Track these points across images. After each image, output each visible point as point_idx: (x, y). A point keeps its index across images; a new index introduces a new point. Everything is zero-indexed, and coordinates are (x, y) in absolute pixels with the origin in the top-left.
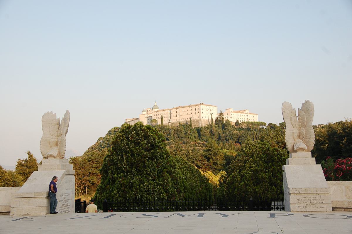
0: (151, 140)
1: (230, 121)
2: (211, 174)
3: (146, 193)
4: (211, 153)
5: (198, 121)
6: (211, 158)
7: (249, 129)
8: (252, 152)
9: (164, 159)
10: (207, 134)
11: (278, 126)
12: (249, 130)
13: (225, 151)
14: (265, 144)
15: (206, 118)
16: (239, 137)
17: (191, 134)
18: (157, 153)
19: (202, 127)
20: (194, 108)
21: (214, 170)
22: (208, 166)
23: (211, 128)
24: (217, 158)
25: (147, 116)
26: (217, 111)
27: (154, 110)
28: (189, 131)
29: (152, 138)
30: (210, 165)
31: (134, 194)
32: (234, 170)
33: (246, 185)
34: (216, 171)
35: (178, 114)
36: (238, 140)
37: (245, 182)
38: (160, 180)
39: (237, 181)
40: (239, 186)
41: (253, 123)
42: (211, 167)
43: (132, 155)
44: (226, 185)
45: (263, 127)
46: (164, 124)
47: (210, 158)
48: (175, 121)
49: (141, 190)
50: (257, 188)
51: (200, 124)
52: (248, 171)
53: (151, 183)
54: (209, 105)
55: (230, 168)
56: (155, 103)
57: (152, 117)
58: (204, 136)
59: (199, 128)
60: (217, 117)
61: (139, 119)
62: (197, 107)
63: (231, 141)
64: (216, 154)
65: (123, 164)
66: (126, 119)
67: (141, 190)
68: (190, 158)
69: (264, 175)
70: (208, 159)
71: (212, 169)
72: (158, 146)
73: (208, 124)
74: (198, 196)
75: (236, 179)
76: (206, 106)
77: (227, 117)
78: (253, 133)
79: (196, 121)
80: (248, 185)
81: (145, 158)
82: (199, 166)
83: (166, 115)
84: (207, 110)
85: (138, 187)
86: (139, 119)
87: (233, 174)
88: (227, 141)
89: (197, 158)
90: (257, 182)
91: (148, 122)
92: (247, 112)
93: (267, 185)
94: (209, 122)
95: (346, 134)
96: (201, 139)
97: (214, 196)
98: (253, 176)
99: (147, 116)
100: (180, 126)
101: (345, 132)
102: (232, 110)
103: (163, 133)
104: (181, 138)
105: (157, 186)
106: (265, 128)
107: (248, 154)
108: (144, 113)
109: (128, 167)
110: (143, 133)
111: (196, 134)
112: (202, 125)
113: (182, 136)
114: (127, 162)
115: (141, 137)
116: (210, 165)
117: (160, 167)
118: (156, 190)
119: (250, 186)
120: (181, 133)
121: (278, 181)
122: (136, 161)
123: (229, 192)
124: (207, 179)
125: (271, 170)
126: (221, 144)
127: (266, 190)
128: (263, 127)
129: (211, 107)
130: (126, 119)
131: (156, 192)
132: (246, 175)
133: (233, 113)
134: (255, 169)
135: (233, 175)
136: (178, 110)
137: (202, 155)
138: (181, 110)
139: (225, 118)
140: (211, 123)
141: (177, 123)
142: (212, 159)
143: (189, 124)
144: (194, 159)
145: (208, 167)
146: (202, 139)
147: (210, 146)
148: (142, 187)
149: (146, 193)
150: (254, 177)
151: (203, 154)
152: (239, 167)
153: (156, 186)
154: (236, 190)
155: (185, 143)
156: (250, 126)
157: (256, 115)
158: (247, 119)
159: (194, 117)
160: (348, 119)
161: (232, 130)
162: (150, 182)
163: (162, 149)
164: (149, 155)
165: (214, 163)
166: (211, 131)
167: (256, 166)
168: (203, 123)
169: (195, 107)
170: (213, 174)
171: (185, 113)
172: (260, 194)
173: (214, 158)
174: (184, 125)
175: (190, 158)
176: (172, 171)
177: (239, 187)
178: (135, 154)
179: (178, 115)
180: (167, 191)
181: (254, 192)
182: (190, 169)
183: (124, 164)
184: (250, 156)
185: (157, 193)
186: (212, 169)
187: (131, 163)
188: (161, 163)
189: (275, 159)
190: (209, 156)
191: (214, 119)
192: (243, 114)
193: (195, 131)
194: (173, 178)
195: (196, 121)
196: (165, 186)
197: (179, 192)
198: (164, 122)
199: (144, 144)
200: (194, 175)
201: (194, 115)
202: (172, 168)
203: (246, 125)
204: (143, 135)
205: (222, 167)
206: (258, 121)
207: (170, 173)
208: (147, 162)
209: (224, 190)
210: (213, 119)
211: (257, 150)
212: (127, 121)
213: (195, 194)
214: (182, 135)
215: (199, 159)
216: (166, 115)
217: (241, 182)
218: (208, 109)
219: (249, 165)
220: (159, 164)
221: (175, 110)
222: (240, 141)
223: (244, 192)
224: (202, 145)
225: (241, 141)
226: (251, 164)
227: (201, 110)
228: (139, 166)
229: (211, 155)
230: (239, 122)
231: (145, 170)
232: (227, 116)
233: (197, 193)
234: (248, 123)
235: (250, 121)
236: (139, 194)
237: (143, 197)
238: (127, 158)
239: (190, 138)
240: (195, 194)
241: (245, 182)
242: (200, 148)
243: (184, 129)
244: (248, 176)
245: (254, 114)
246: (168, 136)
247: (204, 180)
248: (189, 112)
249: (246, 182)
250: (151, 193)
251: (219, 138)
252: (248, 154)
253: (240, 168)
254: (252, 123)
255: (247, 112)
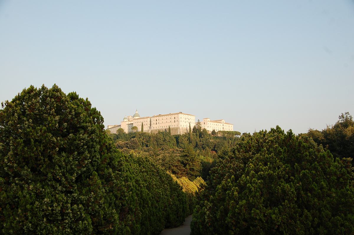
0: (70, 116)
1: (207, 130)
2: (186, 180)
3: (45, 220)
4: (188, 158)
5: (176, 129)
6: (188, 163)
7: (224, 138)
8: (256, 143)
9: (95, 151)
10: (186, 142)
11: (252, 135)
12: (224, 139)
13: (202, 157)
14: (278, 131)
15: (185, 127)
16: (215, 145)
17: (169, 141)
18: (80, 140)
19: (180, 135)
20: (173, 117)
21: (190, 176)
22: (185, 172)
23: (189, 136)
24: (194, 164)
25: (128, 123)
26: (195, 120)
27: (135, 118)
28: (167, 138)
29: (73, 113)
30: (187, 171)
31: (19, 222)
32: (225, 175)
33: (250, 206)
34: (192, 178)
35: (157, 122)
36: (214, 148)
37: (248, 200)
38: (84, 192)
39: (232, 197)
40: (236, 208)
41: (229, 133)
42: (187, 173)
43: (27, 142)
44: (209, 203)
45: (238, 136)
46: (144, 131)
47: (187, 164)
48: (155, 128)
49: (34, 215)
50: (274, 213)
51: (179, 132)
52: (254, 177)
53: (60, 198)
54: (188, 115)
55: (214, 172)
56: (137, 112)
57: (132, 124)
58: (182, 143)
59: (178, 136)
60: (195, 126)
61: (120, 125)
62: (176, 116)
63: (208, 149)
64: (193, 160)
65: (6, 160)
66: (108, 126)
67: (34, 215)
68: (166, 163)
69: (287, 187)
70: (185, 165)
71: (188, 175)
72: (85, 128)
73: (186, 132)
74: (167, 210)
75: (229, 194)
76: (184, 115)
77: (204, 126)
78: (228, 142)
79: (175, 129)
80: (254, 206)
81: (54, 148)
82: (175, 172)
83: (147, 122)
84: (185, 119)
85: (28, 206)
86: (120, 125)
87: (223, 182)
88: (204, 148)
89: (173, 163)
90: (273, 200)
91: (129, 129)
92: (223, 122)
93: (294, 208)
94: (187, 130)
95: (328, 141)
96: (179, 146)
97: (190, 205)
98: (264, 188)
99: (128, 123)
100: (159, 133)
101: (327, 139)
102: (209, 120)
103: (143, 140)
104: (160, 145)
105: (71, 206)
106: (239, 137)
107: (250, 148)
108: (125, 120)
109: (15, 165)
110: (56, 102)
111: (174, 141)
112: (180, 132)
113: (161, 143)
114: (16, 154)
115: (50, 109)
116: (187, 171)
117: (84, 167)
118: (69, 213)
119: (257, 209)
120: (160, 140)
121: (314, 199)
122: (35, 155)
123: (215, 217)
124: (180, 187)
125: (299, 177)
126: (198, 151)
127: (291, 218)
128: (238, 136)
129: (190, 116)
130: (108, 126)
131: (69, 216)
132: (249, 187)
133: (209, 123)
134: (268, 174)
135: (223, 186)
136: (157, 118)
137: (179, 161)
138: (160, 118)
139: (202, 127)
140: (188, 131)
141: (156, 130)
142: (189, 164)
143: (168, 131)
144: (170, 165)
145: (184, 173)
146: (180, 147)
147: (187, 151)
148: (37, 208)
149: (45, 220)
150: (265, 191)
151: (180, 159)
152: (233, 169)
153: (69, 205)
154: (229, 215)
155: (163, 150)
156: (226, 135)
157: (231, 125)
158: (223, 128)
159: (173, 125)
160: (330, 126)
161: (209, 139)
162: (57, 196)
163: (92, 133)
164: (62, 142)
165: (190, 169)
166: (189, 138)
167: (270, 168)
168: (181, 131)
169: (174, 116)
170: (189, 180)
171: (164, 121)
172: (279, 226)
173: (191, 164)
174: (163, 133)
175: (166, 163)
176: (111, 175)
177: (236, 210)
178: (32, 140)
179: (157, 123)
180: (95, 214)
181: (267, 222)
182: (158, 173)
183: (8, 159)
184: (253, 150)
185: (71, 219)
186: (188, 175)
187: (24, 158)
188: (86, 159)
189: (306, 155)
190: (185, 161)
191: (192, 128)
192: (220, 124)
193: (173, 138)
194: (113, 187)
195: (175, 129)
196: (90, 204)
197: (123, 212)
198: (144, 129)
199: (53, 122)
200: (163, 182)
201: (173, 124)
202: (111, 170)
203: (222, 134)
204: (55, 105)
205: (198, 173)
206: (233, 131)
207: (107, 179)
208: (56, 157)
209: (205, 213)
210: (191, 127)
211: (269, 139)
212: (109, 128)
213: (163, 208)
214: (161, 142)
215: (176, 165)
216: (147, 123)
217: (240, 198)
218: (186, 118)
219: (255, 166)
220: (83, 161)
221: (155, 118)
222: (216, 149)
223: (245, 220)
224: (180, 152)
225: (217, 149)
226: (258, 165)
227: (180, 118)
228: (40, 164)
229: (187, 160)
230: (216, 131)
231: (52, 173)
232: (204, 125)
233: (166, 207)
234: (224, 132)
235: (226, 130)
236: (31, 222)
237: (39, 228)
238: (16, 148)
239: (168, 145)
240: (163, 208)
241: (248, 200)
242: (178, 154)
243: (163, 137)
244: (254, 187)
245: (229, 124)
246: (147, 142)
247: (176, 188)
248: (169, 121)
249: (251, 200)
250: (58, 220)
251: (196, 146)
252: (250, 148)
253: (236, 172)
254: (228, 132)
255: (223, 122)
